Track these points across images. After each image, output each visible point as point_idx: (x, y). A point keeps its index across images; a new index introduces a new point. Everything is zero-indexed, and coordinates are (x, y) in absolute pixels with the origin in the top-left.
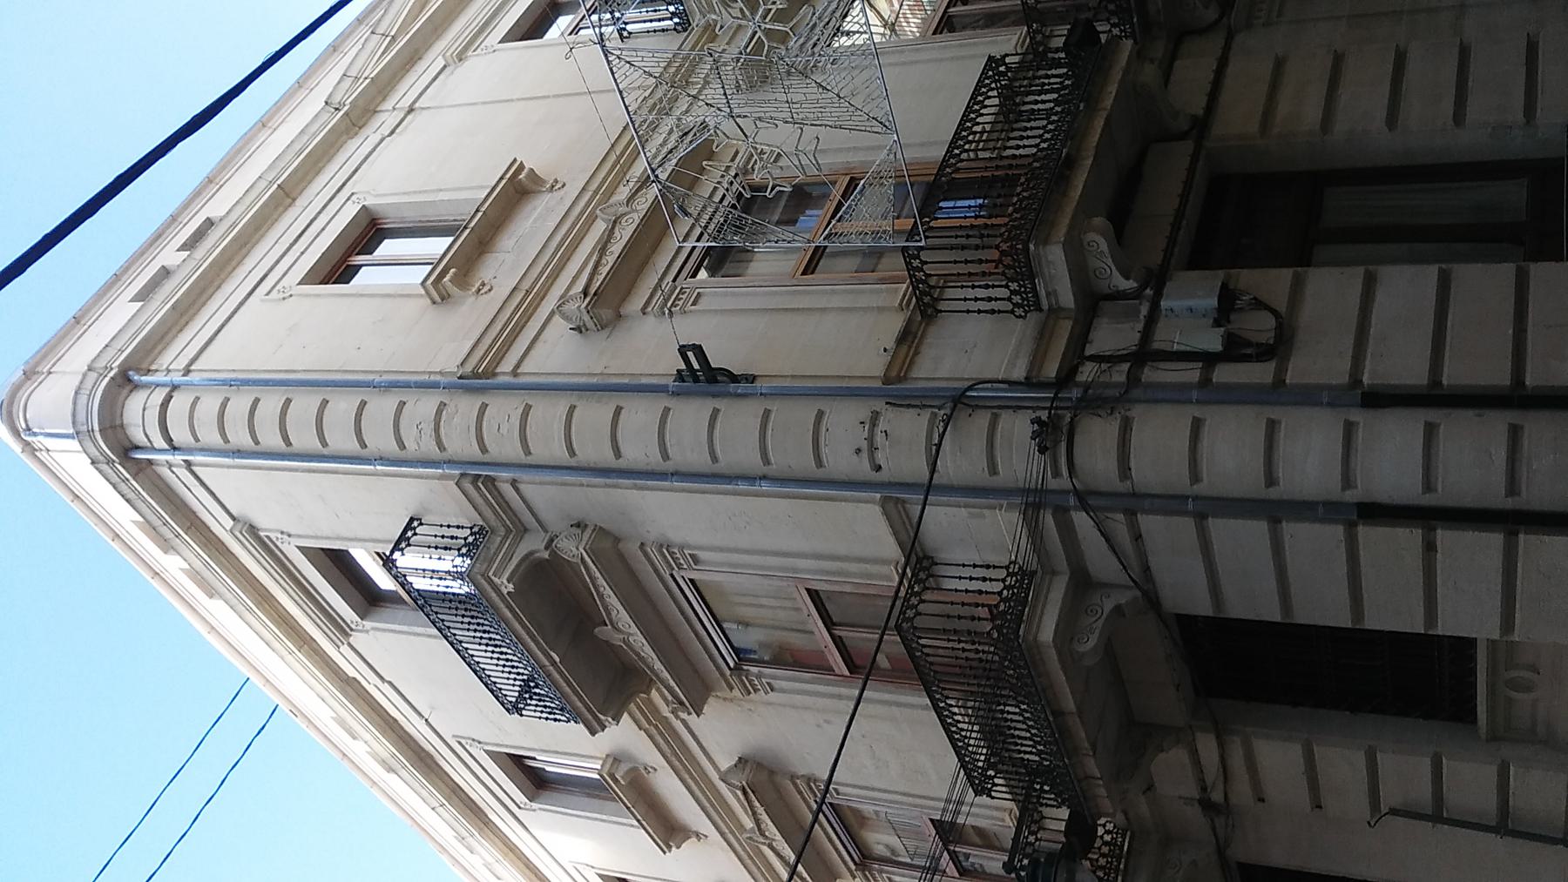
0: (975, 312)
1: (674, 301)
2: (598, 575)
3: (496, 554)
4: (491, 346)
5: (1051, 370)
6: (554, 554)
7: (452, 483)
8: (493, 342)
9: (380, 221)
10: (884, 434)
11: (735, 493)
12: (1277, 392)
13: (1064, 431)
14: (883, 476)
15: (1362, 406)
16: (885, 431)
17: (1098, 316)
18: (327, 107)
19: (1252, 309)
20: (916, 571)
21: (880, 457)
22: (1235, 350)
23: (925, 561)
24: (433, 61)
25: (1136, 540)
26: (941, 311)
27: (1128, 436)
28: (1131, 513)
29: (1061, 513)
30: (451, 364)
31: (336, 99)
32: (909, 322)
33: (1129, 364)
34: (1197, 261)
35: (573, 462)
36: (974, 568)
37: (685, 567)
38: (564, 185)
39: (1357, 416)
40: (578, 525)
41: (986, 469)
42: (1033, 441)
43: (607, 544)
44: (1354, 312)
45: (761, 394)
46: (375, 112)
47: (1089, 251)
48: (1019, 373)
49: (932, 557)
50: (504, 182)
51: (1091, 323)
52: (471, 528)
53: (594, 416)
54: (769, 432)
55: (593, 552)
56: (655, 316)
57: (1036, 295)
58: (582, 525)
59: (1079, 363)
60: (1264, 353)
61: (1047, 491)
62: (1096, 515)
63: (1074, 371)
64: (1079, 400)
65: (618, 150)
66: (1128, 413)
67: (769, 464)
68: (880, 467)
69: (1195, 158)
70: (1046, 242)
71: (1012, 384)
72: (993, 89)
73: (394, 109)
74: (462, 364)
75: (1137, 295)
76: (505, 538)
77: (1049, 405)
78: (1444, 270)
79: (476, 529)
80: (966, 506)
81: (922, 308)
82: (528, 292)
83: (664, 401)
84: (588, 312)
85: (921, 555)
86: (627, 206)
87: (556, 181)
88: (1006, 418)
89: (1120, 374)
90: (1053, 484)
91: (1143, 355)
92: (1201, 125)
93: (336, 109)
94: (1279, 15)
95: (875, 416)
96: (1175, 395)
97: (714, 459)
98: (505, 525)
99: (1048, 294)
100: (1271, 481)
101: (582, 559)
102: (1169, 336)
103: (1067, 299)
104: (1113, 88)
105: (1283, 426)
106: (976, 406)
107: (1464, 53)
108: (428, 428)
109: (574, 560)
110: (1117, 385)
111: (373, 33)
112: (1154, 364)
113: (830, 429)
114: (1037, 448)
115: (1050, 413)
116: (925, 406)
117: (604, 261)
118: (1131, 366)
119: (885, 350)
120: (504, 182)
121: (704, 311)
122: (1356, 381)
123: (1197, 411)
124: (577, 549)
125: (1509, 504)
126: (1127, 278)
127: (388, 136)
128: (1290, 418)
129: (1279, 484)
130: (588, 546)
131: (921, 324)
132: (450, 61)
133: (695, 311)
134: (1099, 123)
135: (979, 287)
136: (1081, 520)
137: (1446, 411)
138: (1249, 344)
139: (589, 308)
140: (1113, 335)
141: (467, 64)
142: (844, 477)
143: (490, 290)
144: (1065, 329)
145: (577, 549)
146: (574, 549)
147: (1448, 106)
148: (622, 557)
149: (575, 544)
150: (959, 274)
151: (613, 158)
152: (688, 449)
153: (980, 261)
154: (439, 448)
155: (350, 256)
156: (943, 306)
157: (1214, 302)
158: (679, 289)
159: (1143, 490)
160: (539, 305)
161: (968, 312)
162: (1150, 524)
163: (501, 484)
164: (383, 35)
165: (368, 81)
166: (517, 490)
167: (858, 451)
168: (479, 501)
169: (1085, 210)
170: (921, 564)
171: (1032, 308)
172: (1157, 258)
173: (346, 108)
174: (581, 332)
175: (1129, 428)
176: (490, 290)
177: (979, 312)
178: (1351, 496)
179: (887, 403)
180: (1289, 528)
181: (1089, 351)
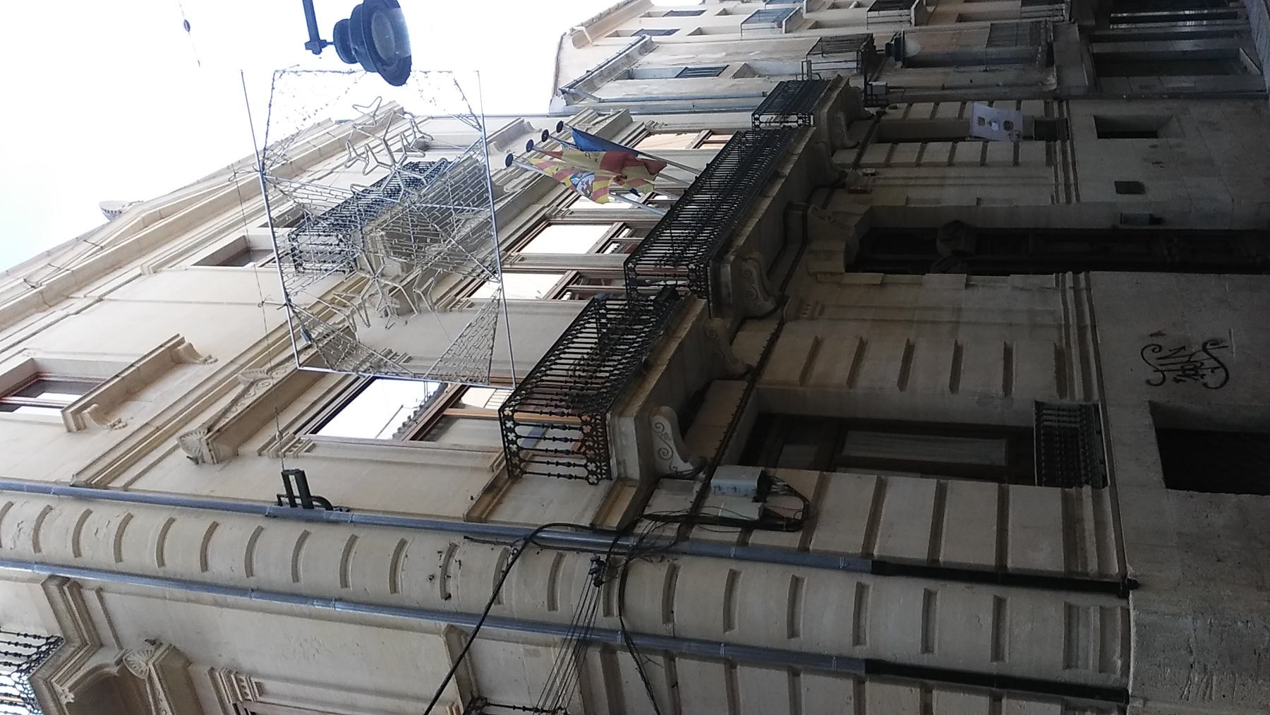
0: (555, 475)
1: (290, 447)
2: (162, 696)
3: (65, 663)
4: (110, 465)
5: (614, 521)
6: (124, 670)
7: (40, 586)
8: (113, 462)
9: (43, 374)
10: (458, 563)
11: (310, 616)
12: (803, 556)
13: (619, 572)
14: (450, 605)
15: (872, 573)
16: (460, 561)
17: (659, 488)
18: (25, 284)
19: (785, 495)
20: (470, 709)
21: (451, 588)
22: (769, 521)
23: (480, 701)
24: (133, 269)
25: (673, 687)
26: (526, 473)
27: (673, 582)
28: (670, 658)
29: (608, 652)
30: (68, 478)
31: (34, 280)
32: (497, 479)
33: (679, 524)
34: (746, 460)
35: (161, 572)
36: (524, 710)
37: (250, 697)
38: (216, 361)
39: (869, 580)
40: (153, 643)
41: (546, 603)
42: (590, 576)
43: (178, 664)
44: (869, 505)
45: (352, 522)
46: (68, 298)
47: (655, 431)
48: (586, 522)
49: (486, 699)
50: (163, 349)
51: (652, 493)
52: (48, 639)
53: (191, 528)
54: (352, 554)
55: (162, 669)
56: (269, 457)
57: (608, 465)
58: (158, 643)
59: (638, 520)
60: (792, 526)
61: (593, 628)
62: (640, 658)
63: (634, 524)
64: (635, 548)
65: (271, 340)
66: (675, 562)
67: (346, 586)
68: (450, 596)
69: (747, 393)
70: (621, 415)
71: (578, 528)
72: (593, 318)
73: (85, 297)
74: (77, 474)
75: (693, 476)
76: (80, 649)
77: (608, 550)
78: (941, 485)
79: (52, 640)
80: (525, 642)
81: (510, 468)
82: (158, 429)
83: (261, 521)
84: (208, 444)
85: (476, 695)
86: (267, 374)
87: (210, 357)
88: (569, 558)
89: (671, 531)
90: (601, 621)
91: (692, 519)
92: (754, 373)
93: (33, 287)
94: (820, 314)
95: (452, 549)
96: (716, 552)
97: (296, 577)
98: (81, 636)
99: (618, 463)
100: (793, 632)
101: (150, 677)
102: (716, 506)
103: (634, 471)
104: (687, 326)
105: (805, 582)
106: (544, 545)
107: (958, 351)
108: (28, 528)
109: (142, 677)
110: (668, 538)
111: (85, 241)
112: (701, 526)
113: (409, 556)
114: (593, 582)
115: (608, 557)
116: (497, 543)
117: (234, 409)
118: (680, 526)
119: (472, 498)
120: (163, 349)
121: (316, 458)
122: (867, 554)
123: (734, 565)
124: (147, 664)
125: (993, 668)
126: (685, 461)
127: (73, 314)
128: (811, 577)
129: (799, 636)
130: (157, 663)
131: (507, 481)
132: (146, 271)
133: (307, 457)
134: (674, 346)
135: (563, 464)
136: (626, 660)
137: (942, 583)
138: (782, 518)
139: (209, 441)
140: (667, 502)
141: (159, 276)
142: (415, 605)
143: (124, 427)
144: (628, 495)
145: (147, 664)
146: (143, 664)
147: (946, 378)
148: (190, 682)
149: (145, 658)
150: (547, 450)
151: (265, 344)
152: (271, 568)
153: (566, 440)
154: (34, 548)
155: (6, 396)
156: (534, 468)
157: (754, 484)
158: (297, 439)
159: (683, 634)
160: (166, 440)
161: (549, 475)
162: (686, 667)
163: (87, 591)
164: (93, 244)
165: (68, 272)
166: (101, 599)
167: (432, 578)
168: (61, 606)
169: (656, 399)
170: (475, 704)
171: (604, 476)
172: (711, 454)
173: (41, 288)
174: (197, 463)
175: (675, 575)
176: (124, 427)
177: (559, 476)
178: (861, 652)
179: (465, 537)
180: (806, 680)
181: (647, 512)
